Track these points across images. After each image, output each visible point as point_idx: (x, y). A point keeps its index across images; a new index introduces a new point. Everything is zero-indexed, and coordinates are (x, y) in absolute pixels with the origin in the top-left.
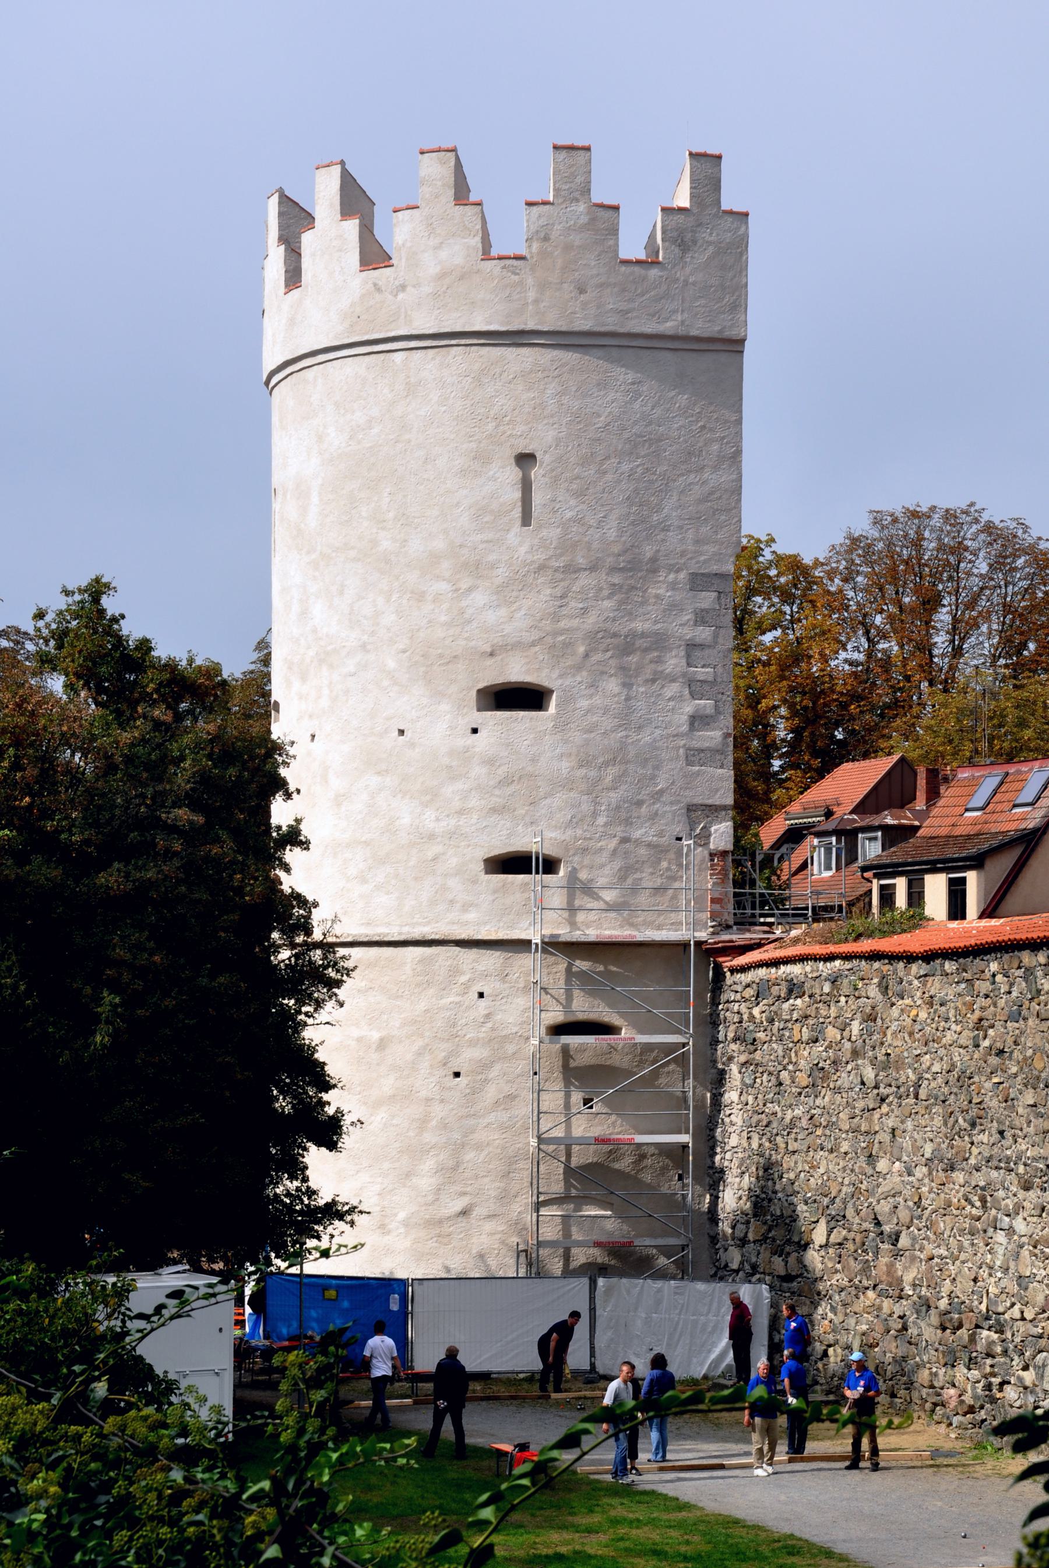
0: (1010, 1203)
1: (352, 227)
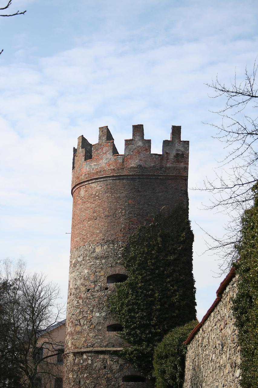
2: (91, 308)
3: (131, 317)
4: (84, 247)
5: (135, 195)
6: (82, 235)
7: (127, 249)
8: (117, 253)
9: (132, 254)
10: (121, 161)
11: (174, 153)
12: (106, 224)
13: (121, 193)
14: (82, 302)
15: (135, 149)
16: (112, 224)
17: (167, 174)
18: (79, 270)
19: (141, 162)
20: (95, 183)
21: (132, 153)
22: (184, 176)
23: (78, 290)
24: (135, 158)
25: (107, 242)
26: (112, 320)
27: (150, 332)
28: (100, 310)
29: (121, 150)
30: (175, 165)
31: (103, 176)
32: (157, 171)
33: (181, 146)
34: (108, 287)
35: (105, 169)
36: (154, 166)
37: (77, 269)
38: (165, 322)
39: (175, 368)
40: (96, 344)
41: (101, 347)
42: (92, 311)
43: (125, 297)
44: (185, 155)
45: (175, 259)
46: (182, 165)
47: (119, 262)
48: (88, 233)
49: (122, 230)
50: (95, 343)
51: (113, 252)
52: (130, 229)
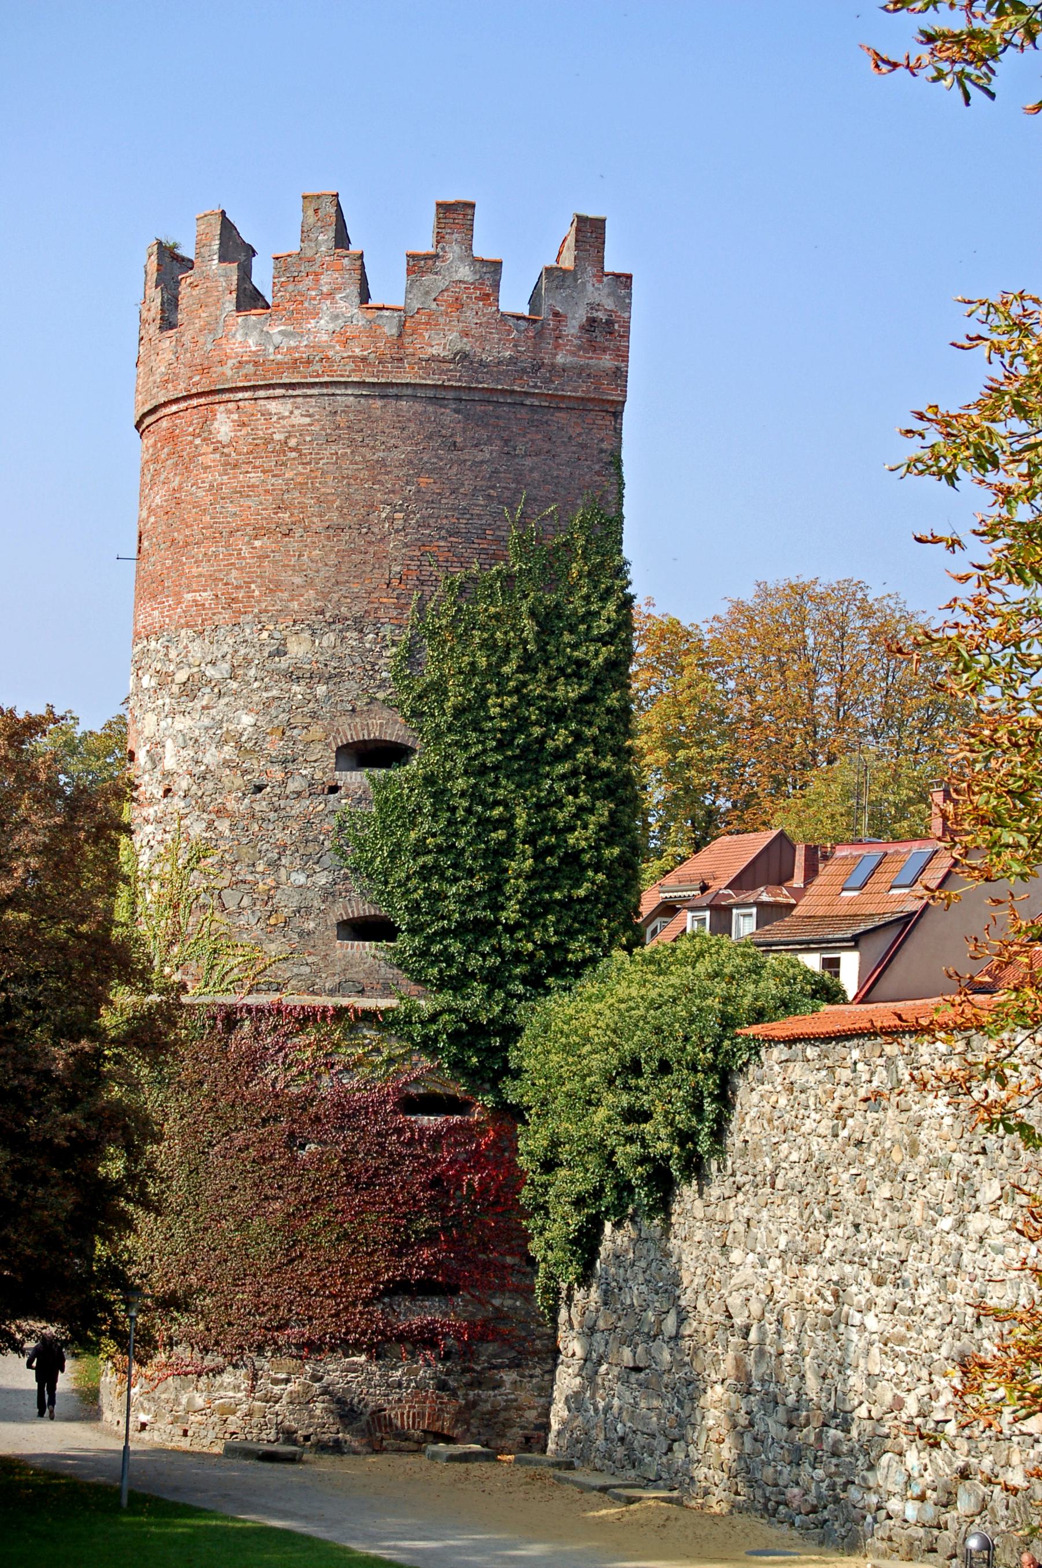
0: (862, 1299)
1: (232, 269)
2: (270, 855)
3: (429, 895)
4: (236, 628)
5: (441, 460)
6: (226, 584)
7: (411, 655)
8: (373, 664)
9: (430, 674)
10: (395, 331)
11: (579, 316)
12: (333, 556)
13: (389, 449)
14: (231, 830)
15: (446, 290)
16: (356, 558)
17: (556, 389)
18: (213, 712)
19: (465, 340)
20: (281, 400)
21: (434, 306)
22: (613, 401)
23: (211, 785)
24: (445, 325)
25: (334, 622)
26: (357, 902)
27: (498, 951)
28: (309, 862)
29: (390, 287)
30: (582, 362)
31: (322, 380)
32: (521, 378)
33: (606, 291)
34: (340, 783)
35: (331, 353)
36: (511, 358)
37: (203, 708)
38: (551, 918)
39: (697, 1109)
40: (293, 982)
41: (314, 993)
42: (274, 865)
43: (404, 825)
44: (616, 326)
45: (584, 699)
46: (607, 361)
47: (381, 695)
48: (254, 582)
49: (395, 583)
50: (289, 979)
51: (357, 660)
52: (422, 583)
